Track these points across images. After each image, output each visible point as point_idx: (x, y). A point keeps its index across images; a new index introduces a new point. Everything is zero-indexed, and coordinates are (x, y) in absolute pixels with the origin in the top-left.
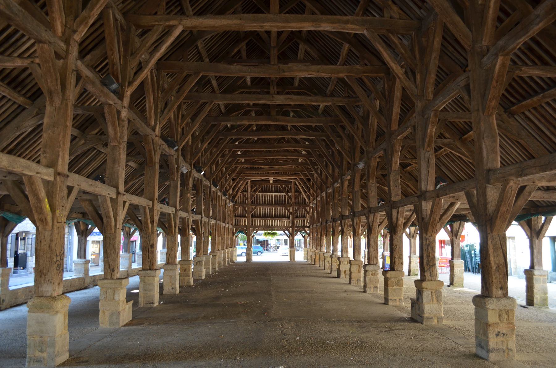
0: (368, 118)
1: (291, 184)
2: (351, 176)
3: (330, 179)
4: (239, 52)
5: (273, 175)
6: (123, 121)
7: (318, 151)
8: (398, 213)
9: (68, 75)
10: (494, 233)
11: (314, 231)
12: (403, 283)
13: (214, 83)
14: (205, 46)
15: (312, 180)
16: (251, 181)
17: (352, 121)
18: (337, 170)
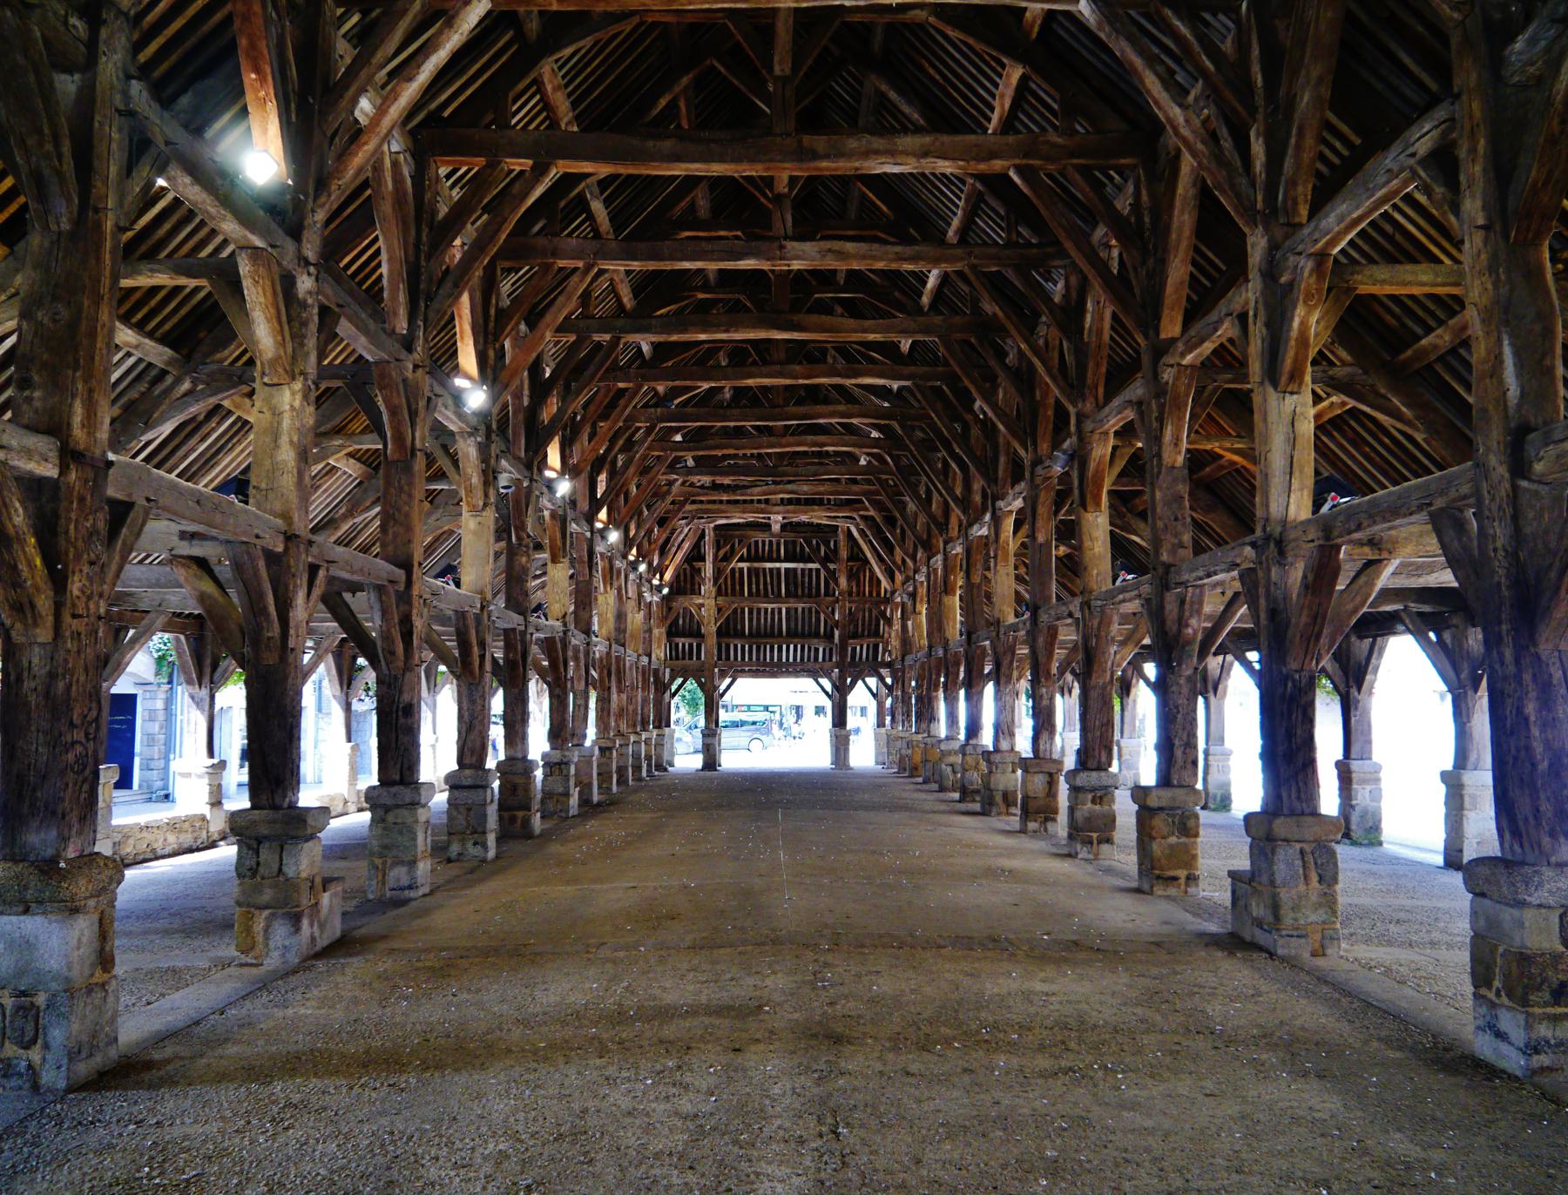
0: (1082, 310)
1: (837, 536)
2: (1024, 498)
3: (957, 513)
6: (304, 305)
7: (923, 430)
9: (96, 124)
10: (1542, 647)
11: (907, 675)
12: (1197, 826)
14: (566, 86)
15: (900, 522)
16: (717, 528)
18: (978, 485)
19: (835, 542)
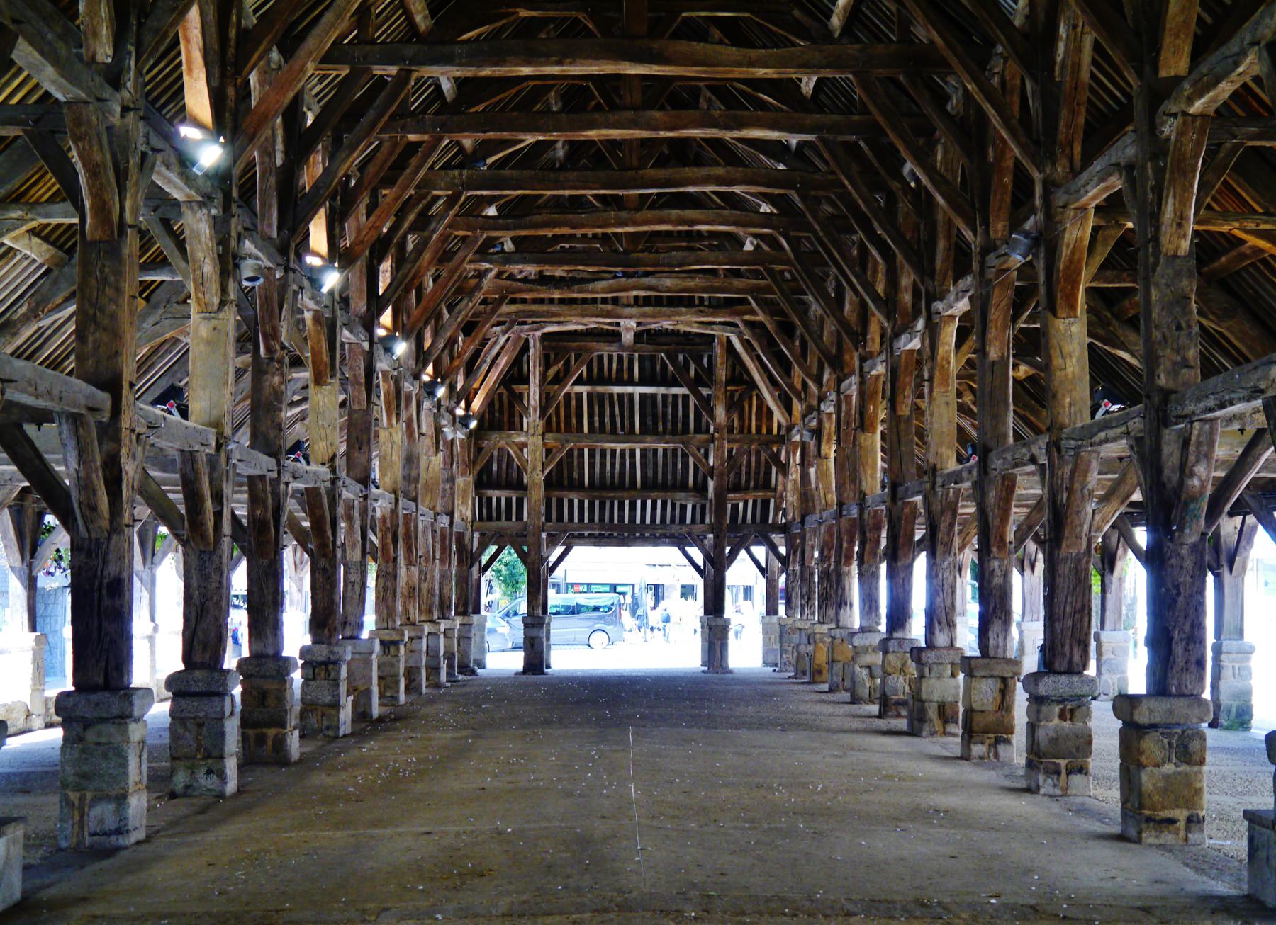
0: (1052, 37)
2: (971, 298)
5: (634, 310)
11: (809, 543)
12: (1203, 749)
16: (546, 337)
18: (907, 279)
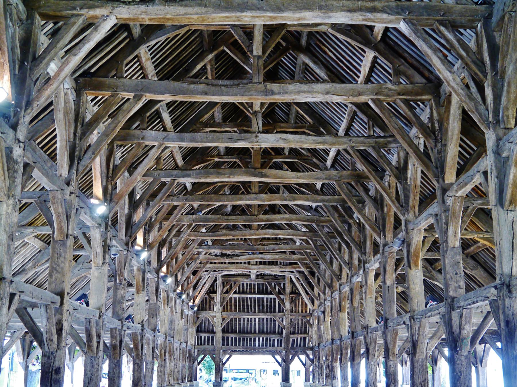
2: (380, 263)
4: (204, 68)
6: (16, 162)
8: (461, 317)
11: (321, 354)
13: (166, 116)
14: (152, 58)
16: (223, 276)
17: (380, 173)
18: (356, 255)
19: (284, 284)
